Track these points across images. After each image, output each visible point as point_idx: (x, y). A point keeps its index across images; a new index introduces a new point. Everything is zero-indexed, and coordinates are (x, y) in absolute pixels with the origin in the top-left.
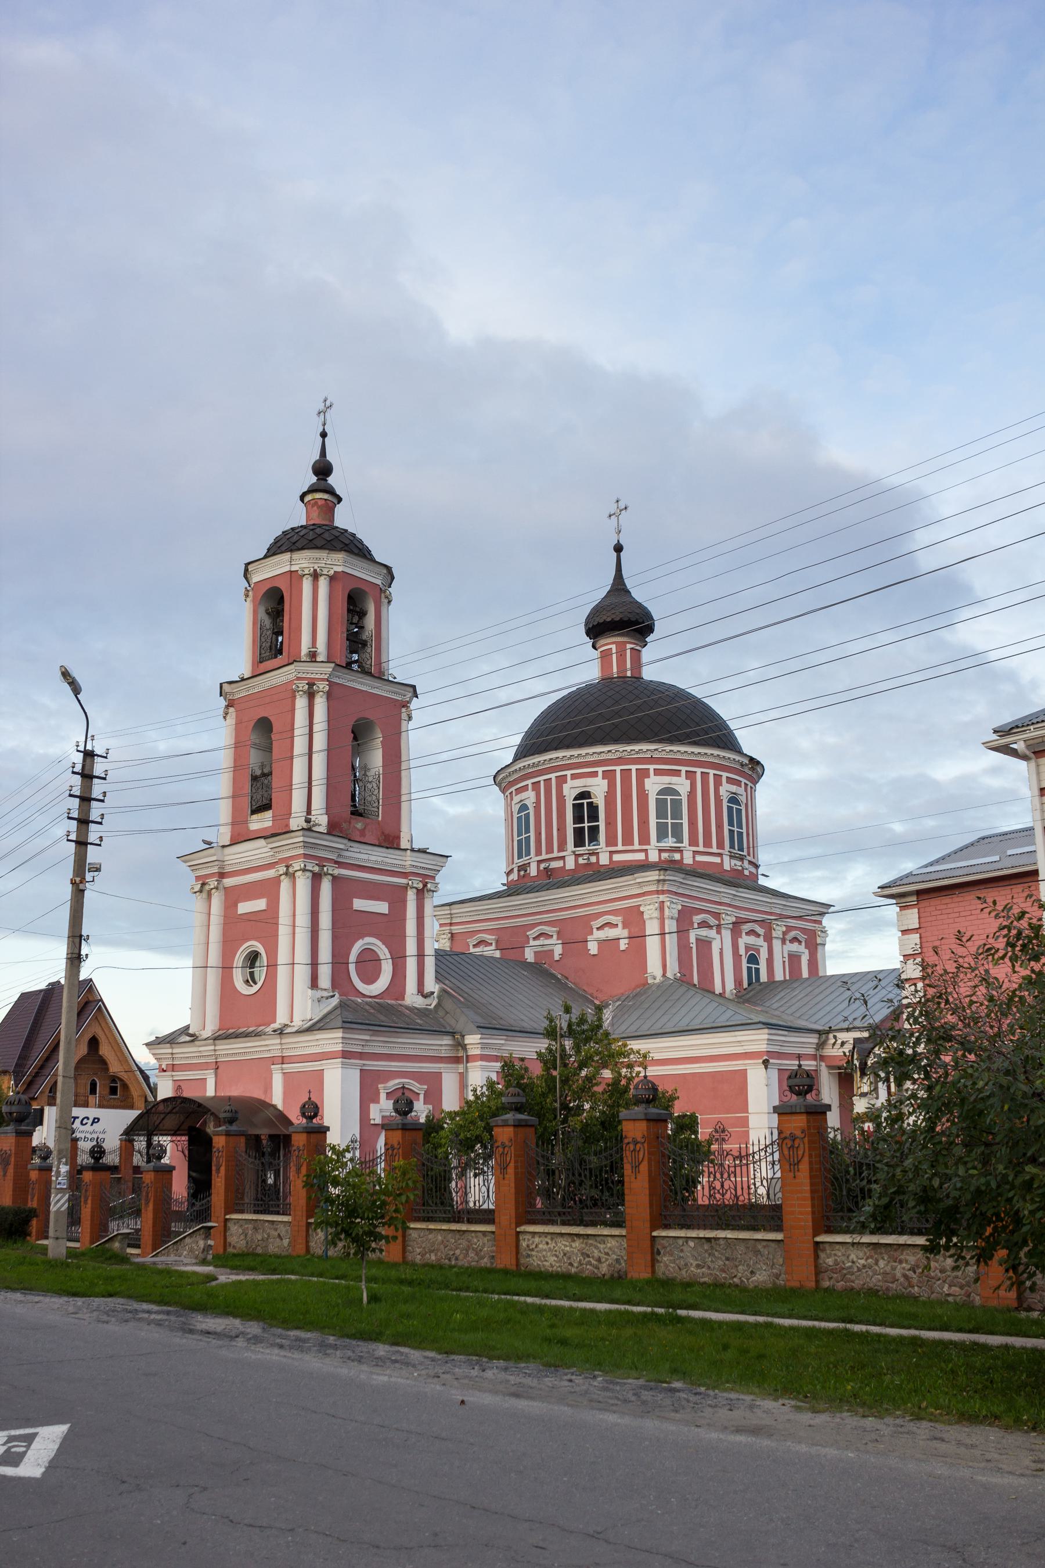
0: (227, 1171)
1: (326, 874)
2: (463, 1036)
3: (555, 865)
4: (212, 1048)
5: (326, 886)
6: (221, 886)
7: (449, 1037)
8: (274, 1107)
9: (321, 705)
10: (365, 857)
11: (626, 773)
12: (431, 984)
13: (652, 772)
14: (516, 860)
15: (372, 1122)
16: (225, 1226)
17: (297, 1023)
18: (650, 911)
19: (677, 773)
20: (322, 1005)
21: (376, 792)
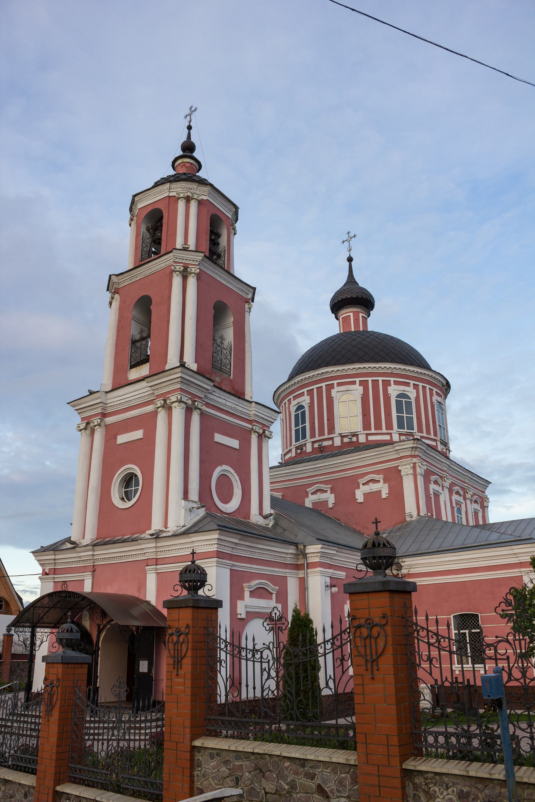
0: (194, 665)
1: (197, 408)
2: (305, 546)
3: (325, 443)
4: (91, 553)
5: (196, 418)
6: (103, 424)
7: (293, 547)
8: (148, 603)
9: (192, 282)
10: (223, 402)
11: (375, 383)
12: (267, 509)
13: (392, 383)
14: (293, 442)
15: (239, 617)
16: (192, 759)
17: (172, 527)
18: (406, 470)
19: (408, 384)
20: (193, 515)
21: (229, 357)
